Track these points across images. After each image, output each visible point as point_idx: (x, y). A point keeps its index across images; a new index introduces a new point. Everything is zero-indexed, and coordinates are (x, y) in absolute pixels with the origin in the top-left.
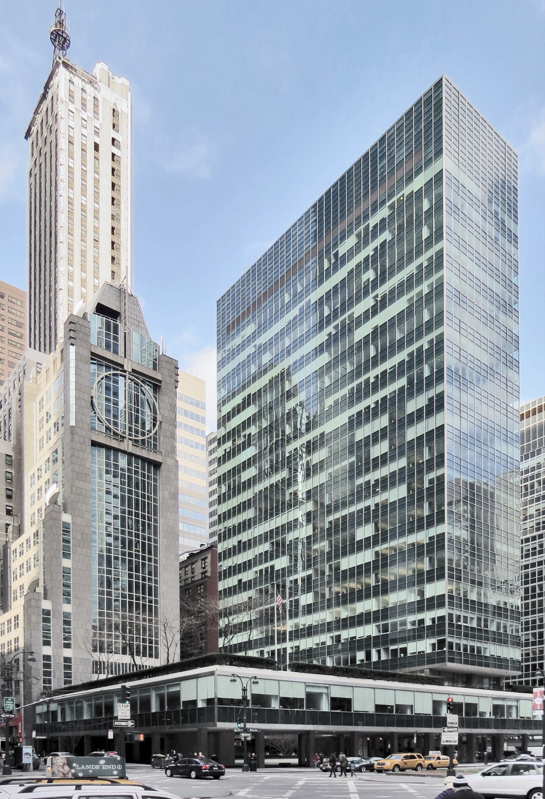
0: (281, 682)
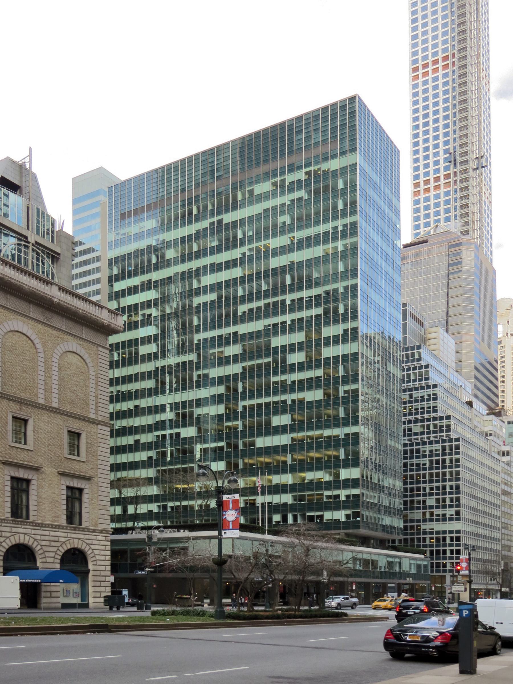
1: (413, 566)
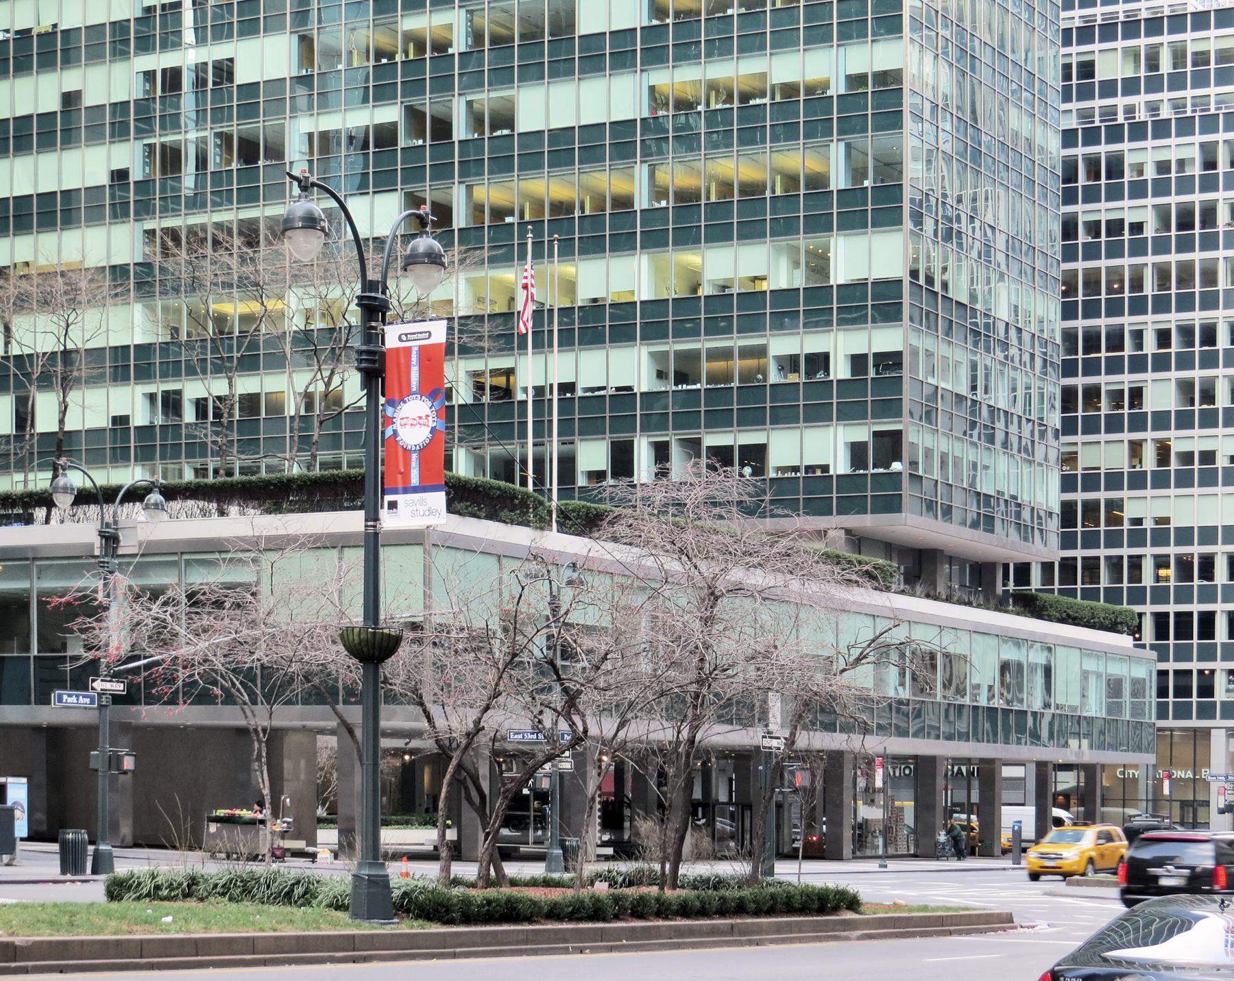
0: (504, 561)
1: (1092, 680)
